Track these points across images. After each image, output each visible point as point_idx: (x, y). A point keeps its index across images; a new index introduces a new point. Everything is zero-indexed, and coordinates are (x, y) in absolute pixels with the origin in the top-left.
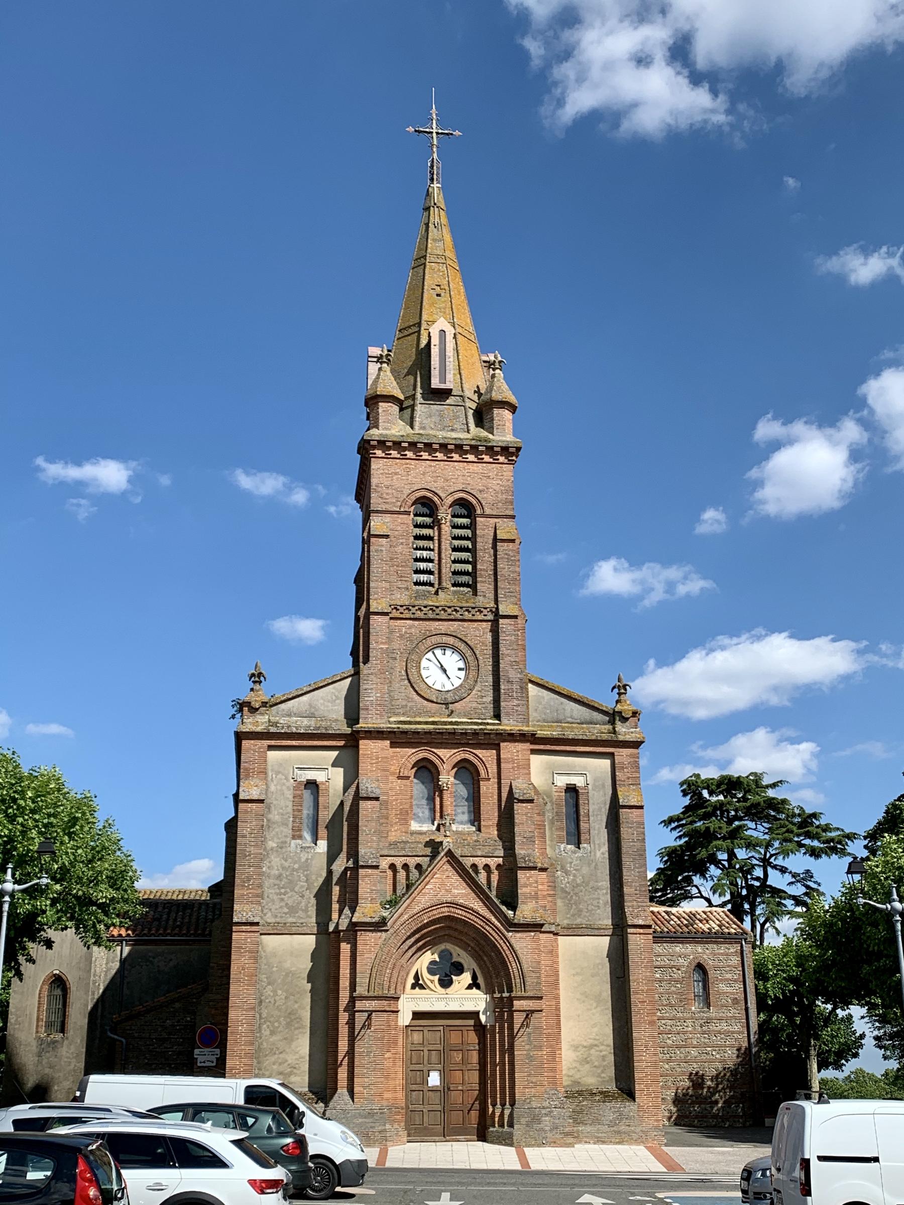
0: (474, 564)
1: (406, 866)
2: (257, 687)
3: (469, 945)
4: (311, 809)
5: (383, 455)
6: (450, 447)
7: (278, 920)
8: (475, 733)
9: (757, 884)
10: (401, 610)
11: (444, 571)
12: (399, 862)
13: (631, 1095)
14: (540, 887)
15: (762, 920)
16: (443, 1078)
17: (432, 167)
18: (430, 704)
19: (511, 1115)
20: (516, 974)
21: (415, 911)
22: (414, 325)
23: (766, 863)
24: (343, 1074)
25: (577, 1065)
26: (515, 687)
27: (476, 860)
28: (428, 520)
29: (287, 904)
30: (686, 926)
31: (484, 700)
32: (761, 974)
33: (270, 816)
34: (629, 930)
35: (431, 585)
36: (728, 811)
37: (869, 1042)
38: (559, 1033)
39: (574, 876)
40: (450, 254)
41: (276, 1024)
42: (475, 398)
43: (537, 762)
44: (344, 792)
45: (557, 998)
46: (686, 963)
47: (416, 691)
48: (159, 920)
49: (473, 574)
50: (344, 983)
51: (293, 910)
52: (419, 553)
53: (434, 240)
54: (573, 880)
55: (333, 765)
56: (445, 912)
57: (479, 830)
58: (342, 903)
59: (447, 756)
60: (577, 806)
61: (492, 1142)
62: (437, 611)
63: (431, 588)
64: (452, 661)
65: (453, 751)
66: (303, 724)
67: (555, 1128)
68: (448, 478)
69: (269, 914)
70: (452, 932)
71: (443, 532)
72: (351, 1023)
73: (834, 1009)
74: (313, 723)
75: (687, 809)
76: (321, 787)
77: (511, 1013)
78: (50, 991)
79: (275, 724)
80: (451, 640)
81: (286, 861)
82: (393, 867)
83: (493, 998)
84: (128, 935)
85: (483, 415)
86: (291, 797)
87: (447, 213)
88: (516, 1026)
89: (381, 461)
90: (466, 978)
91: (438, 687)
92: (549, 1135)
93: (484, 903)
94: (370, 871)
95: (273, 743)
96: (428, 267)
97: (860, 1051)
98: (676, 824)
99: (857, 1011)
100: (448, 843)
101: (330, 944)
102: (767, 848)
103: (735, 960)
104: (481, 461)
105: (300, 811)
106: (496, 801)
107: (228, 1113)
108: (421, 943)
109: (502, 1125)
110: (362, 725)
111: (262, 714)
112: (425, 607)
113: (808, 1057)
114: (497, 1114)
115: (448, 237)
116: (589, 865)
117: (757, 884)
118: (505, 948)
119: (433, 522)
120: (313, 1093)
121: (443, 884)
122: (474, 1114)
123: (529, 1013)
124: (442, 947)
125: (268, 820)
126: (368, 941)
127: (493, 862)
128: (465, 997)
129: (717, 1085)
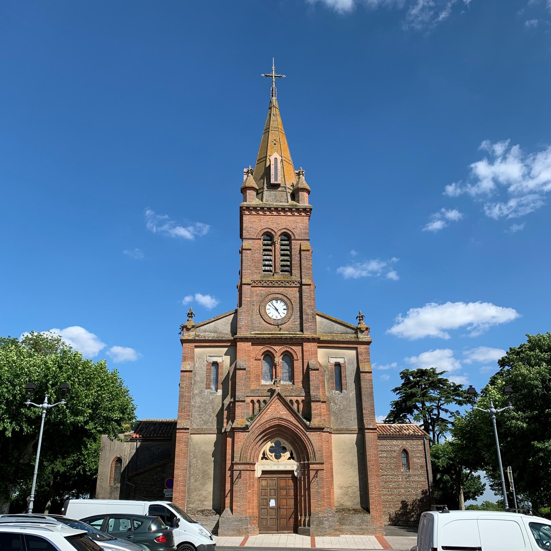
0: (291, 261)
1: (259, 401)
2: (190, 319)
3: (287, 439)
6: (279, 209)
7: (199, 427)
8: (291, 338)
9: (435, 417)
10: (257, 282)
12: (255, 399)
13: (368, 511)
14: (322, 410)
15: (438, 433)
16: (277, 502)
17: (273, 90)
18: (270, 326)
19: (309, 521)
20: (311, 452)
21: (262, 422)
23: (439, 408)
26: (310, 317)
27: (292, 398)
28: (269, 242)
30: (398, 432)
32: (435, 456)
33: (196, 378)
35: (271, 271)
36: (421, 385)
37: (487, 487)
38: (333, 481)
39: (340, 405)
40: (281, 127)
42: (292, 188)
43: (321, 352)
44: (230, 366)
45: (331, 464)
48: (155, 430)
49: (290, 266)
50: (229, 457)
51: (206, 423)
52: (265, 257)
55: (225, 355)
56: (277, 422)
57: (294, 384)
59: (278, 350)
60: (340, 372)
61: (300, 534)
62: (274, 283)
64: (280, 306)
65: (279, 347)
66: (211, 336)
68: (278, 223)
69: (195, 425)
70: (280, 432)
72: (232, 476)
73: (471, 472)
75: (403, 384)
77: (309, 471)
79: (198, 336)
80: (280, 296)
82: (252, 401)
83: (300, 464)
85: (294, 196)
88: (311, 477)
89: (248, 216)
91: (274, 317)
92: (328, 530)
95: (197, 344)
99: (481, 473)
100: (278, 389)
101: (223, 438)
103: (421, 447)
105: (209, 376)
107: (128, 519)
109: (304, 526)
110: (238, 335)
111: (192, 331)
113: (460, 494)
114: (303, 520)
115: (279, 120)
116: (346, 400)
117: (435, 417)
120: (215, 510)
121: (275, 409)
122: (292, 520)
123: (317, 471)
124: (276, 439)
125: (195, 380)
126: (240, 437)
127: (300, 399)
128: (287, 463)
129: (413, 507)
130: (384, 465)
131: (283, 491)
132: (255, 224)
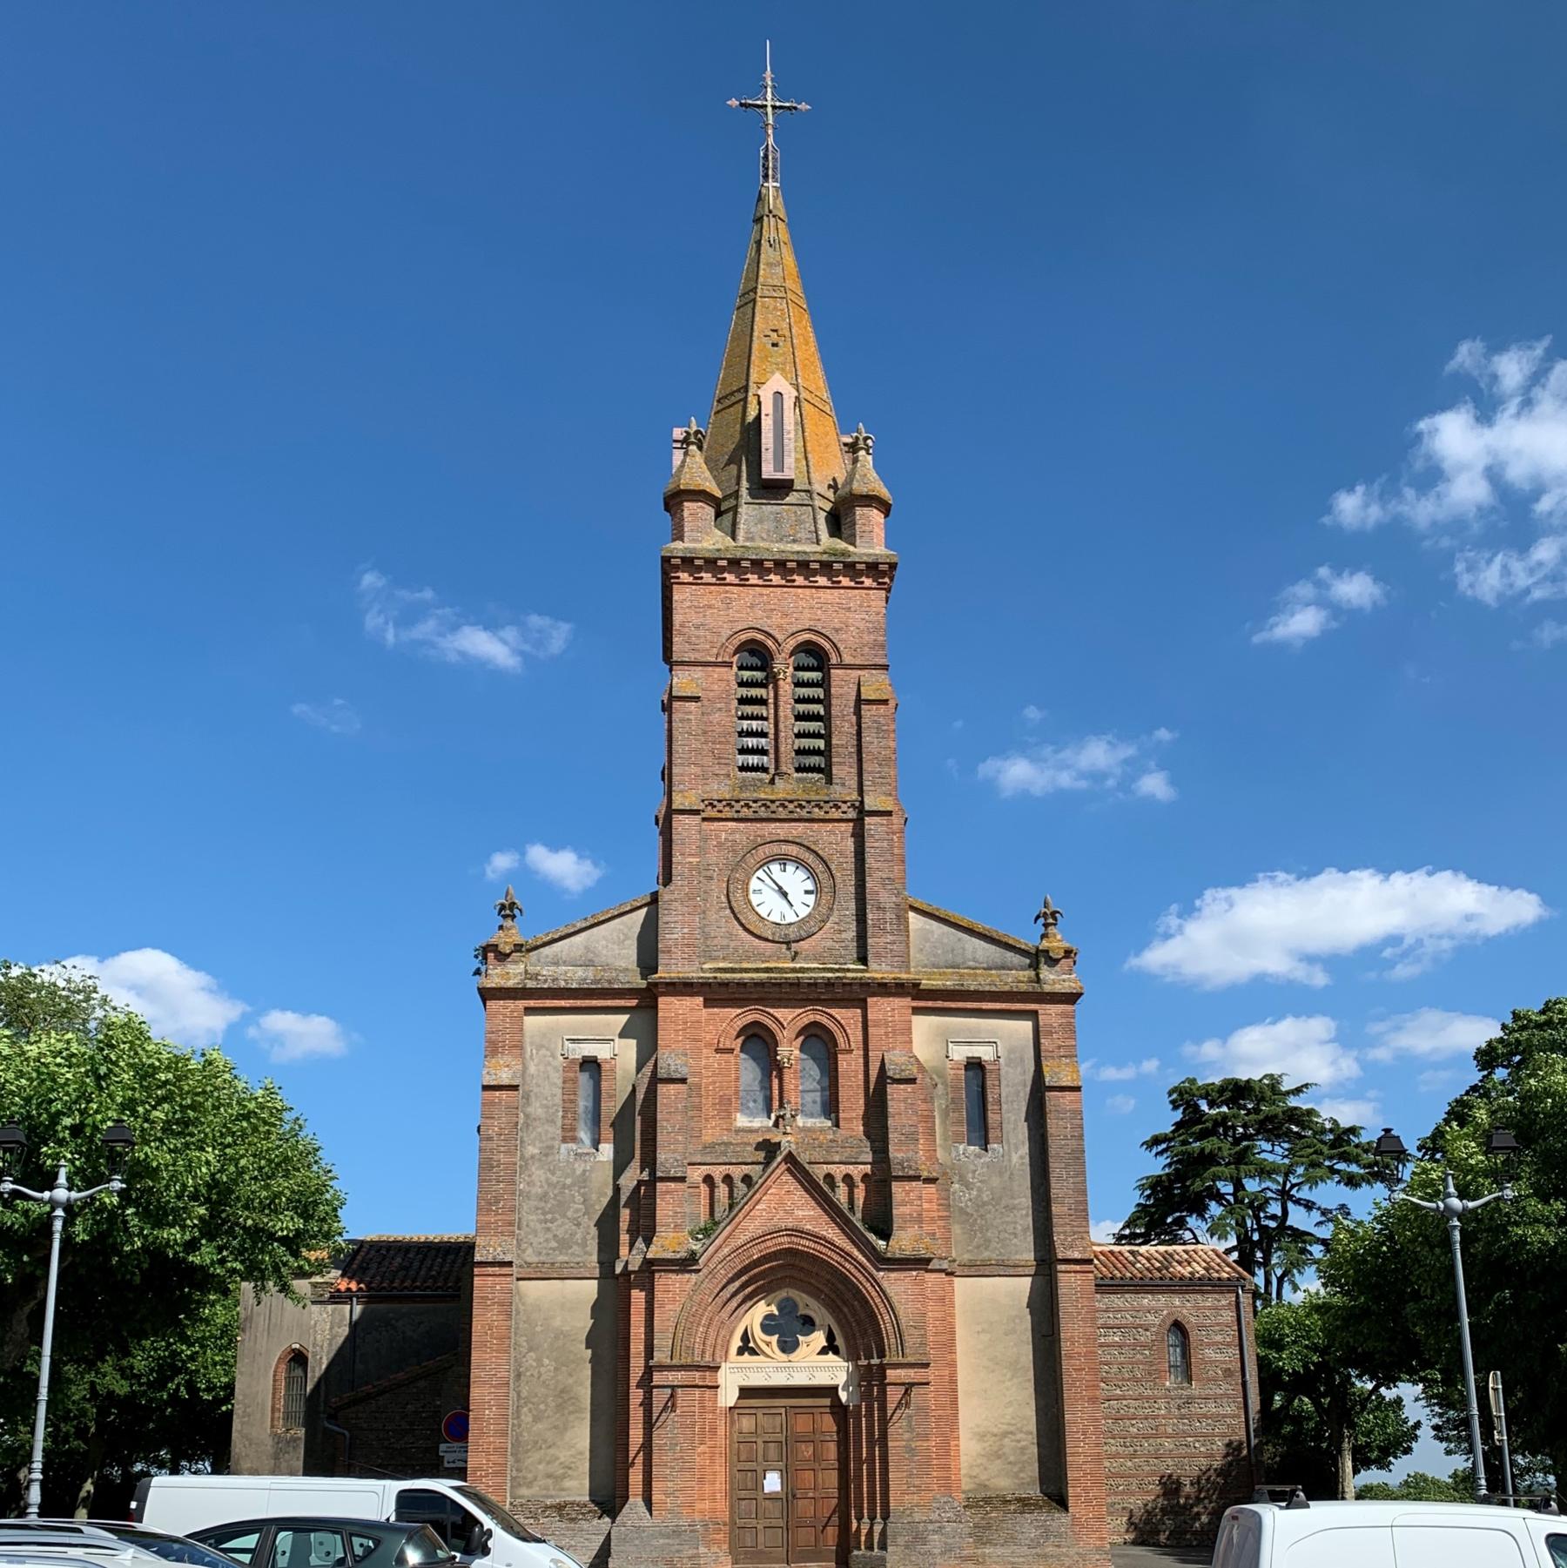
0: (827, 737)
1: (728, 1179)
2: (509, 923)
3: (817, 1289)
4: (591, 1099)
5: (691, 579)
6: (790, 565)
7: (542, 1258)
8: (829, 984)
9: (1273, 1224)
10: (720, 806)
11: (782, 749)
12: (718, 1172)
13: (1059, 1500)
14: (925, 1206)
15: (1279, 1272)
17: (766, 157)
18: (763, 944)
19: (883, 1533)
22: (738, 391)
23: (1285, 1196)
24: (636, 1477)
25: (984, 1461)
26: (888, 915)
27: (832, 1169)
28: (759, 675)
30: (1159, 1270)
31: (844, 935)
32: (1271, 1341)
33: (529, 1110)
34: (1061, 1267)
35: (765, 770)
36: (1234, 1128)
37: (1426, 1433)
38: (956, 1415)
39: (980, 1190)
40: (794, 284)
41: (542, 1407)
42: (830, 494)
43: (923, 1026)
45: (953, 1365)
47: (742, 925)
48: (407, 1269)
49: (826, 753)
51: (564, 1245)
52: (745, 724)
53: (769, 265)
54: (979, 1196)
55: (621, 1035)
56: (785, 1242)
57: (837, 1125)
58: (634, 1233)
59: (788, 1020)
62: (773, 807)
63: (764, 775)
64: (795, 880)
65: (795, 1010)
66: (576, 976)
67: (947, 1550)
68: (788, 612)
69: (530, 1251)
71: (781, 692)
72: (647, 1404)
74: (590, 974)
75: (1179, 1125)
76: (605, 1067)
77: (883, 1387)
78: (289, 1370)
79: (535, 977)
80: (793, 850)
82: (708, 1180)
83: (857, 1366)
84: (360, 1289)
85: (839, 521)
86: (559, 1082)
87: (788, 225)
88: (891, 1407)
89: (688, 589)
90: (819, 1339)
91: (775, 918)
93: (842, 1229)
94: (672, 1185)
95: (532, 1003)
96: (759, 304)
97: (1414, 1445)
98: (1164, 1146)
99: (1408, 1391)
100: (788, 1142)
101: (618, 1291)
102: (1286, 1176)
103: (1229, 1316)
104: (836, 586)
105: (572, 1101)
106: (861, 1083)
108: (750, 1289)
109: (870, 1547)
110: (663, 974)
111: (515, 962)
113: (1340, 1451)
114: (864, 1532)
115: (789, 260)
116: (1001, 1174)
117: (1273, 1224)
118: (874, 1294)
119: (766, 678)
120: (597, 1504)
121: (781, 1203)
122: (832, 1532)
123: (909, 1387)
124: (783, 1294)
125: (527, 1116)
126: (670, 1287)
128: (816, 1365)
129: (1200, 1491)
130: (1115, 1369)
131: (803, 1446)
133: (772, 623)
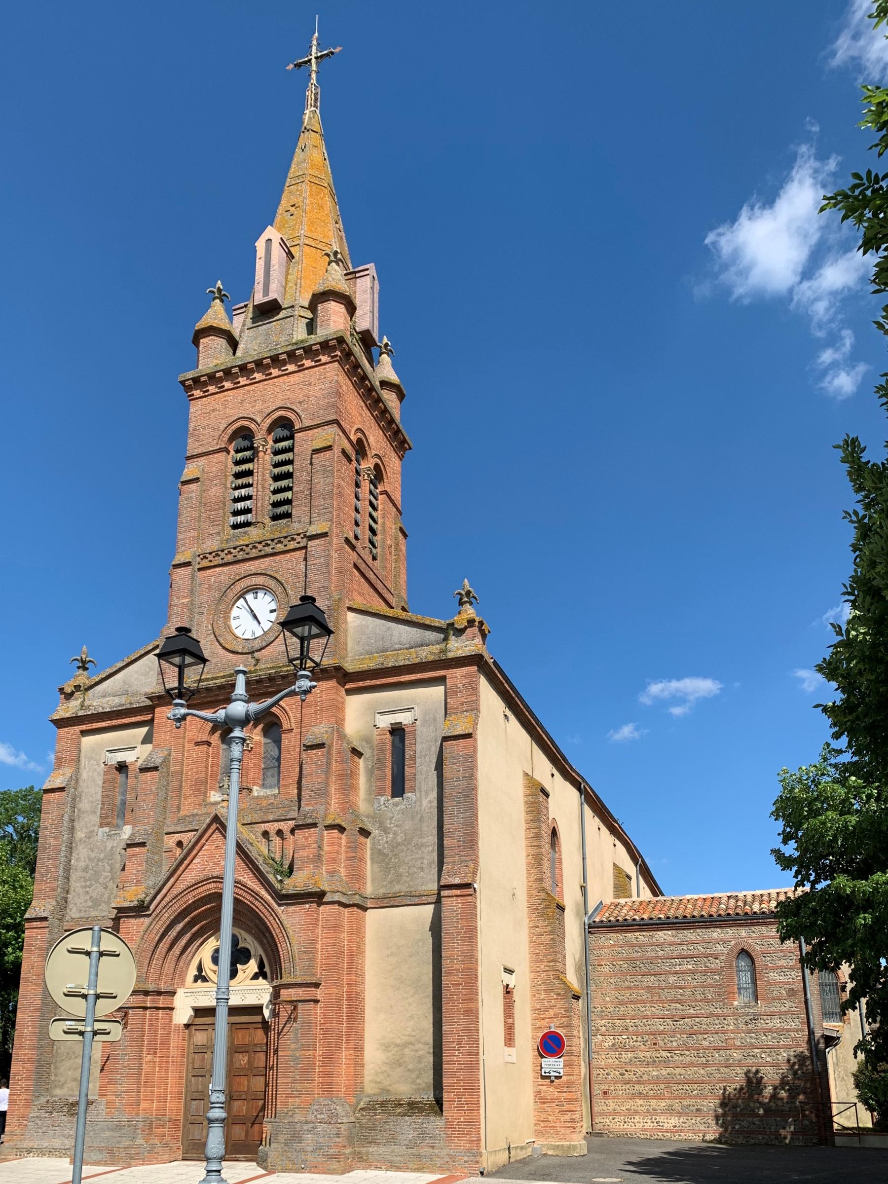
7: (82, 915)
28: (248, 454)
29: (91, 897)
39: (395, 834)
46: (725, 951)
47: (221, 644)
54: (394, 838)
67: (318, 1148)
69: (74, 910)
80: (260, 580)
81: (92, 851)
86: (100, 783)
91: (248, 636)
94: (137, 849)
95: (84, 727)
112: (235, 548)
116: (413, 818)
118: (275, 926)
121: (211, 857)
123: (294, 1003)
130: (688, 992)
131: (241, 1056)
132: (211, 417)
133: (247, 410)
